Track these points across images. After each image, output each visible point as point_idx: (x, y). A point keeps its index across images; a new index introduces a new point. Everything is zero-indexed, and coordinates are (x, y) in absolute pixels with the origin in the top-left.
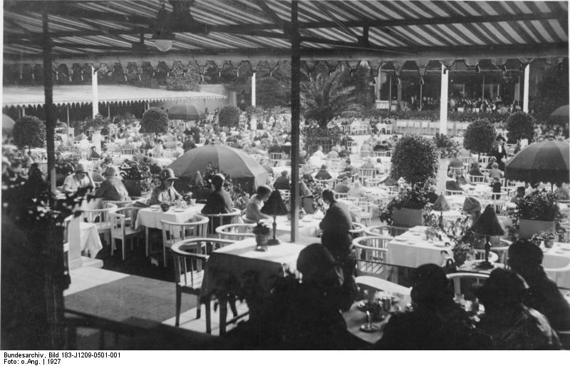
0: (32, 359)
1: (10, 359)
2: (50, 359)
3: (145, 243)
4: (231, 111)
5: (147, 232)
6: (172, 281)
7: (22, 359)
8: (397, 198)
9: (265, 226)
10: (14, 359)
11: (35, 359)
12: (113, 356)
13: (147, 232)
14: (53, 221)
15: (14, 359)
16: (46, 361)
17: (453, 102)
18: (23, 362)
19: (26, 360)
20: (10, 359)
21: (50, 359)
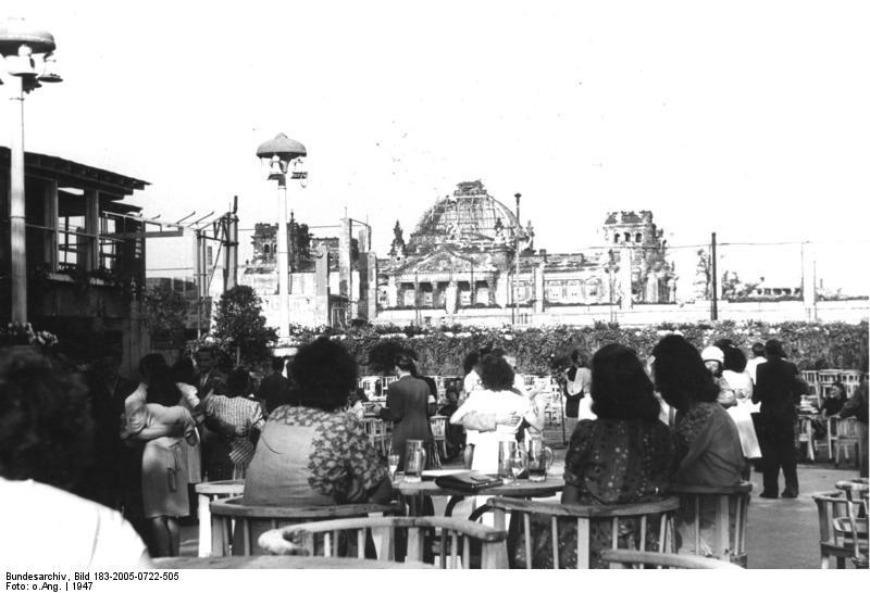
0: (48, 582)
1: (15, 582)
2: (76, 582)
3: (552, 550)
4: (791, 327)
5: (172, 283)
6: (407, 532)
7: (34, 582)
8: (508, 245)
9: (222, 297)
10: (21, 582)
11: (52, 582)
12: (167, 577)
13: (172, 283)
14: (544, 552)
15: (21, 582)
16: (71, 586)
17: (523, 559)
18: (35, 587)
19: (40, 583)
20: (15, 582)
21: (76, 582)
